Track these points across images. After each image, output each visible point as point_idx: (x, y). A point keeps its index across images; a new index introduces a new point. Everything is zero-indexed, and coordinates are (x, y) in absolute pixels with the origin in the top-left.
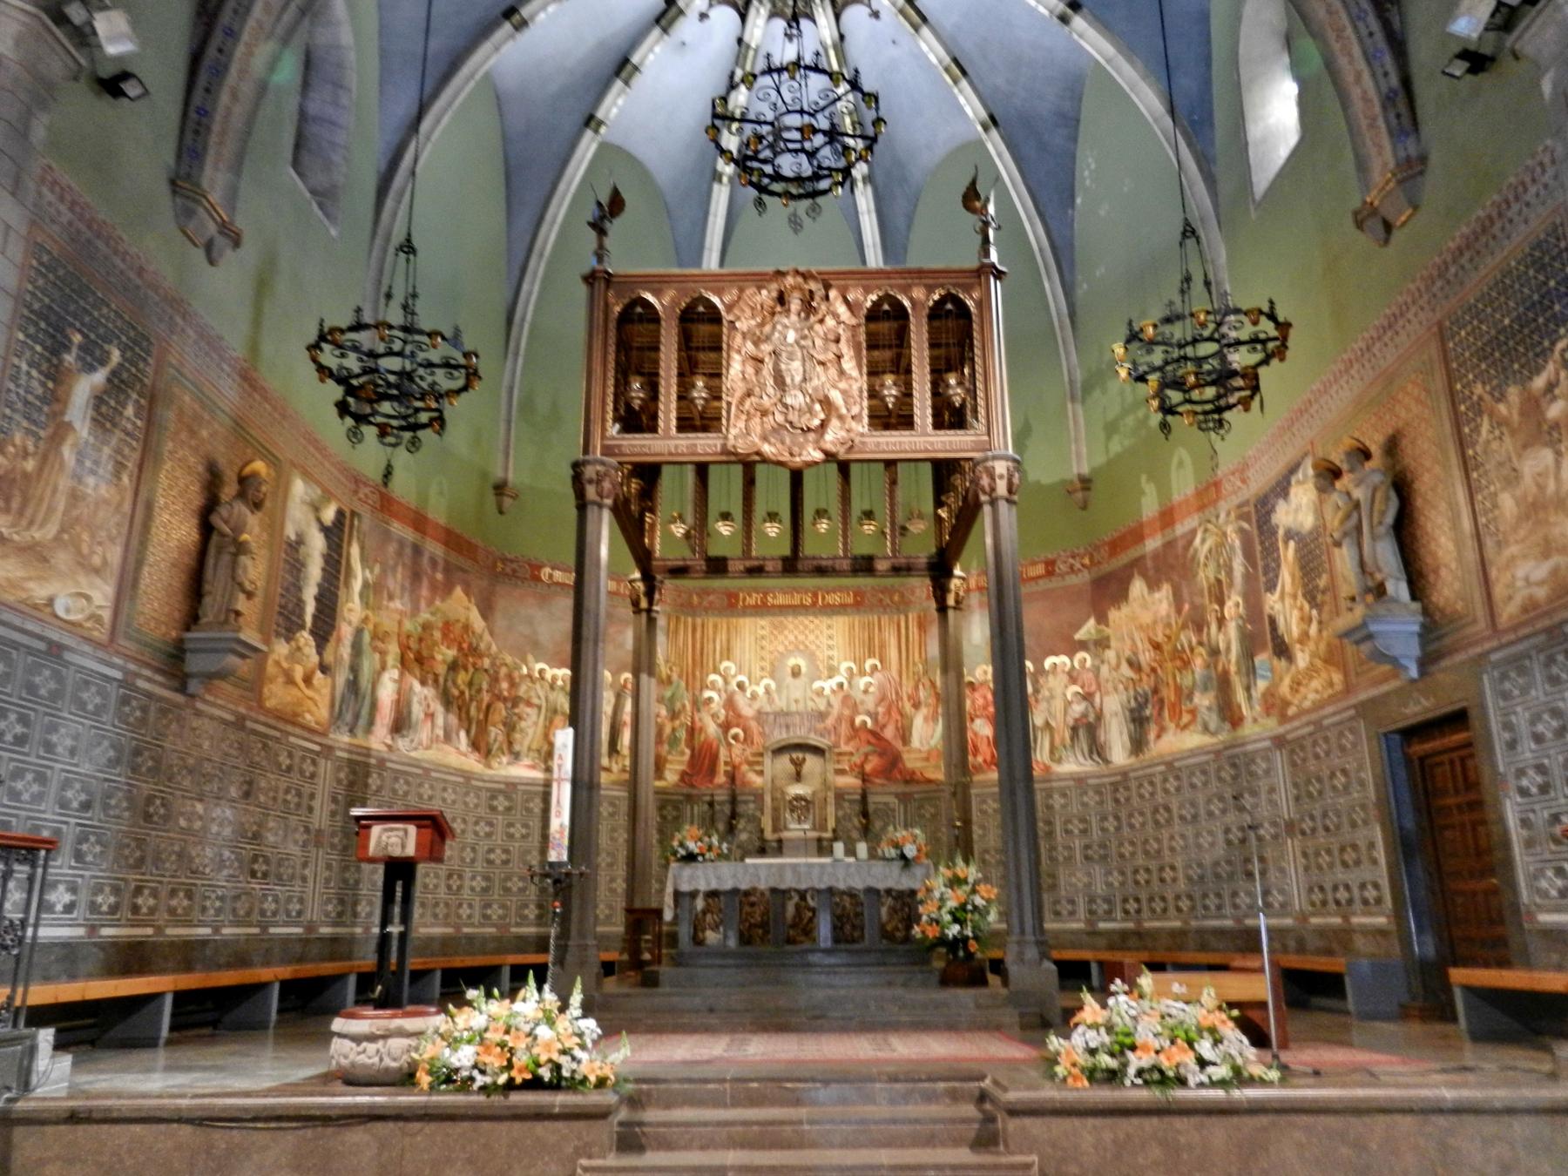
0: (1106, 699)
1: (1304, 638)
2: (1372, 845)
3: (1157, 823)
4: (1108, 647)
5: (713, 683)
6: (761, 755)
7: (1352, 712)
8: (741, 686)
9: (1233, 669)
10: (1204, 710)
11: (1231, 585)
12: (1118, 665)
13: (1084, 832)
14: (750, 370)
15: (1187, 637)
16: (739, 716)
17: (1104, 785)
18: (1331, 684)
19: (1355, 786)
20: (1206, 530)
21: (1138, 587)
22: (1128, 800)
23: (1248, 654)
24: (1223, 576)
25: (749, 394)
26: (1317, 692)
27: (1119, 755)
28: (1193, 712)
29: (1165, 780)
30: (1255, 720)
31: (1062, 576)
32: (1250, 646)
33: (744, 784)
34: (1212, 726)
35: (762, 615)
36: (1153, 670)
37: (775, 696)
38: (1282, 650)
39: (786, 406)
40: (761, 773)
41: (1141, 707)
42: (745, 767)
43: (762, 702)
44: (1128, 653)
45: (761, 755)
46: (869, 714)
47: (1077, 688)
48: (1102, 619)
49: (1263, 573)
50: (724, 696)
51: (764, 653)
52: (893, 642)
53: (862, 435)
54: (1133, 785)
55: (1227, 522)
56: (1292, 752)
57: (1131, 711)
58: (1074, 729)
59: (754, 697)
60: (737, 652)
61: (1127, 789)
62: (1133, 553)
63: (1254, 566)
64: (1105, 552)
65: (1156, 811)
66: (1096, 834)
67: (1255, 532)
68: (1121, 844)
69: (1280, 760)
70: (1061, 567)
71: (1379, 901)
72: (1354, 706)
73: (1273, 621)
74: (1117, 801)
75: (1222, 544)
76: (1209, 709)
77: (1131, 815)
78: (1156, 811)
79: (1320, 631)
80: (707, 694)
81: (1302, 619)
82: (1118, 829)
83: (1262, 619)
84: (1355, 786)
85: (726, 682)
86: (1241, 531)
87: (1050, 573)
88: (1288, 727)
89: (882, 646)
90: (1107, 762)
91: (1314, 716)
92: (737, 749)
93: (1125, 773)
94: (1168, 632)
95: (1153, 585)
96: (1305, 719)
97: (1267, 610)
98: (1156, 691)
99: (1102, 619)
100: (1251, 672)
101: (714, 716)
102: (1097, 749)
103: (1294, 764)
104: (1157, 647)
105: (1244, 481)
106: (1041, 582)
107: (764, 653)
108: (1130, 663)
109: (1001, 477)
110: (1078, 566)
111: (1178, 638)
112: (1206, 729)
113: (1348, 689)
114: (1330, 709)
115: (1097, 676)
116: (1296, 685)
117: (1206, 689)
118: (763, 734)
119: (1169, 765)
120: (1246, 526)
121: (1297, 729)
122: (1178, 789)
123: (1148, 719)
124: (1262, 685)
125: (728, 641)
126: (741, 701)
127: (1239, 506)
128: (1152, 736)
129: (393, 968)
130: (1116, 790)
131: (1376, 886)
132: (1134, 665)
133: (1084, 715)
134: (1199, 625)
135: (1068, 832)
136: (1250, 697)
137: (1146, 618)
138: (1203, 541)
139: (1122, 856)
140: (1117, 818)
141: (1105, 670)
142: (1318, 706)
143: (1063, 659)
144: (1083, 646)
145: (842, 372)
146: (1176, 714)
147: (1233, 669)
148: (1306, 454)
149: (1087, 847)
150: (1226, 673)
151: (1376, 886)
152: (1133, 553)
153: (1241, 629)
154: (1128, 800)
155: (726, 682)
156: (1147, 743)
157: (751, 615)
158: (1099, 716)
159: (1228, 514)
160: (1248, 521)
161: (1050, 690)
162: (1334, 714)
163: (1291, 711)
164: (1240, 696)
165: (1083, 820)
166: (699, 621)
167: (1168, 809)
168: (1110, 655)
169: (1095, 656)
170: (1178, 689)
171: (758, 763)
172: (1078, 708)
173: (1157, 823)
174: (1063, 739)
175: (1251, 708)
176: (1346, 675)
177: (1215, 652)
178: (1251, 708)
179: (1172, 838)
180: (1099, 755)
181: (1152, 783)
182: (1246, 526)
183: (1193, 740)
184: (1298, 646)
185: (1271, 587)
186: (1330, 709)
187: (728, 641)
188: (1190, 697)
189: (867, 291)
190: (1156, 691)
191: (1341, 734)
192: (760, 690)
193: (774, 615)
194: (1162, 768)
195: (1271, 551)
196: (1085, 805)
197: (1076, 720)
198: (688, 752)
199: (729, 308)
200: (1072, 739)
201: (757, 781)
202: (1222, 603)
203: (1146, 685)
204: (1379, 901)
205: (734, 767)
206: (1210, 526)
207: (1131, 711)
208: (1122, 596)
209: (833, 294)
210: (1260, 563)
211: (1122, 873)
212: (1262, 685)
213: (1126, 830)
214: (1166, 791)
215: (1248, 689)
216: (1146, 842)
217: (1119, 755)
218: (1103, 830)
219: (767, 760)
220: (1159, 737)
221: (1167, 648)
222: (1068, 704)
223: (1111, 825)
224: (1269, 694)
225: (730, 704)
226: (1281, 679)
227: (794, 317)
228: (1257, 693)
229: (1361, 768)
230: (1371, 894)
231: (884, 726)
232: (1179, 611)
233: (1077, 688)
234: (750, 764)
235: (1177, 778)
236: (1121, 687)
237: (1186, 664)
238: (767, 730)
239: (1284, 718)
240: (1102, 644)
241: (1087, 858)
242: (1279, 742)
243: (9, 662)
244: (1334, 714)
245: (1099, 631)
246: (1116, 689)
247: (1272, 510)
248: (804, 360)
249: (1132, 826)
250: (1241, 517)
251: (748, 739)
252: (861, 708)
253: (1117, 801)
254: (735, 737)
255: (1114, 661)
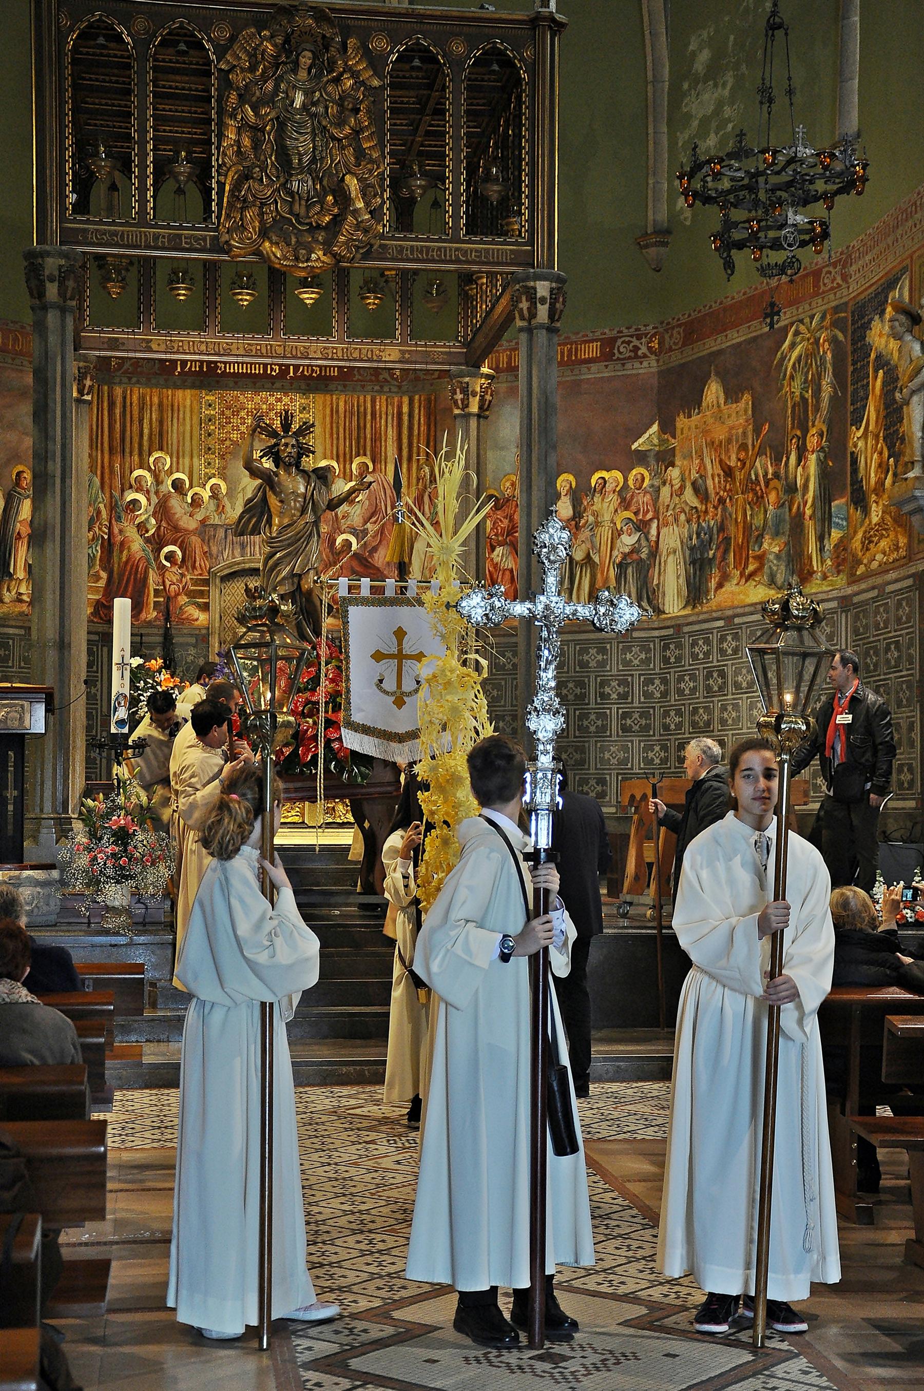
0: (664, 531)
1: (880, 488)
2: (911, 728)
3: (708, 688)
4: (673, 464)
5: (139, 479)
6: (206, 582)
7: (910, 582)
8: (177, 485)
9: (808, 512)
10: (771, 557)
11: (817, 409)
12: (682, 488)
13: (623, 696)
14: (246, 142)
15: (763, 466)
16: (176, 528)
17: (651, 639)
18: (897, 548)
19: (905, 664)
20: (797, 333)
21: (713, 391)
22: (679, 659)
23: (826, 497)
24: (809, 395)
25: (246, 176)
26: (884, 553)
27: (673, 604)
28: (761, 558)
29: (723, 639)
30: (825, 577)
31: (623, 361)
32: (829, 486)
33: (182, 621)
34: (780, 579)
35: (210, 388)
36: (722, 501)
37: (226, 501)
38: (860, 500)
39: (291, 193)
40: (205, 607)
41: (704, 546)
42: (183, 599)
43: (208, 508)
44: (694, 475)
45: (206, 582)
46: (354, 532)
47: (628, 514)
48: (668, 427)
49: (847, 412)
50: (155, 500)
51: (211, 442)
52: (391, 433)
53: (382, 236)
54: (687, 641)
55: (820, 328)
56: (856, 618)
57: (692, 549)
58: (622, 567)
59: (196, 502)
60: (173, 437)
61: (679, 646)
62: (713, 344)
63: (844, 392)
64: (677, 335)
65: (709, 675)
66: (637, 699)
67: (849, 348)
68: (666, 714)
69: (844, 622)
70: (624, 350)
71: (912, 783)
72: (912, 576)
73: (854, 462)
74: (666, 660)
75: (811, 354)
76: (778, 557)
77: (681, 679)
78: (709, 675)
79: (894, 482)
80: (130, 496)
81: (880, 465)
82: (665, 694)
83: (845, 454)
84: (905, 664)
85: (158, 482)
86: (834, 341)
87: (607, 356)
88: (855, 588)
89: (377, 438)
90: (659, 611)
91: (879, 580)
92: (173, 573)
93: (678, 626)
94: (742, 455)
95: (732, 395)
96: (871, 582)
97: (851, 448)
98: (722, 528)
99: (668, 427)
100: (825, 520)
101: (142, 528)
102: (647, 595)
103: (856, 632)
104: (729, 472)
105: (845, 278)
106: (594, 367)
107: (211, 442)
108: (696, 489)
109: (543, 300)
110: (643, 350)
111: (753, 466)
112: (772, 582)
113: (910, 558)
114: (892, 575)
115: (656, 500)
116: (868, 541)
117: (777, 534)
118: (207, 554)
119: (729, 619)
120: (841, 336)
121: (863, 592)
122: (736, 651)
123: (711, 561)
124: (836, 534)
125: (161, 422)
126: (177, 506)
127: (836, 310)
128: (713, 584)
129: (10, 833)
130: (666, 647)
131: (911, 770)
132: (700, 491)
133: (635, 550)
134: (778, 456)
135: (603, 696)
136: (822, 549)
137: (720, 434)
138: (793, 346)
139: (666, 727)
140: (665, 681)
141: (665, 491)
142: (884, 569)
143: (614, 477)
144: (641, 458)
145: (360, 154)
146: (742, 562)
147: (808, 512)
148: (904, 270)
149: (625, 715)
150: (800, 515)
151: (911, 770)
152: (713, 344)
153: (821, 464)
154: (679, 659)
155: (158, 482)
156: (707, 592)
157: (193, 386)
158: (654, 553)
159: (823, 318)
160: (844, 332)
161: (596, 515)
162: (897, 581)
163: (861, 570)
164: (812, 547)
165: (623, 683)
166: (118, 391)
167: (722, 674)
168: (674, 473)
169: (656, 474)
170: (748, 528)
171: (201, 594)
172: (628, 540)
173: (708, 688)
174: (607, 579)
175: (823, 562)
176: (910, 537)
177: (791, 489)
178: (823, 562)
179: (724, 708)
180: (650, 602)
181: (707, 641)
182: (841, 336)
183: (758, 593)
184: (874, 498)
185: (857, 421)
186: (892, 575)
187: (161, 422)
188: (759, 539)
189: (394, 42)
190: (722, 528)
191: (899, 605)
192: (206, 494)
193: (226, 388)
194: (721, 623)
195: (861, 376)
196: (627, 663)
197: (625, 556)
198: (104, 575)
199: (221, 52)
200: (618, 579)
201: (202, 618)
202: (805, 431)
203: (711, 521)
204: (912, 783)
205: (169, 599)
206: (802, 328)
207: (692, 549)
208: (693, 401)
209: (352, 42)
210: (850, 389)
211: (664, 748)
212: (836, 534)
213: (673, 697)
214: (722, 652)
215: (821, 538)
216: (695, 710)
217: (673, 604)
218: (648, 695)
219: (214, 593)
220: (720, 586)
221: (739, 476)
222: (617, 534)
223: (656, 688)
224: (842, 545)
225: (162, 510)
226: (855, 532)
227: (303, 74)
228: (829, 545)
229: (911, 644)
230: (906, 777)
231: (375, 549)
232: (757, 431)
233: (628, 514)
234: (191, 594)
235: (736, 637)
236: (683, 517)
237: (760, 499)
238: (214, 550)
239: (853, 579)
240: (666, 458)
241: (625, 729)
242: (845, 603)
243: (6, 646)
244: (897, 581)
245: (662, 442)
246: (676, 520)
247: (867, 326)
248: (314, 134)
249: (680, 692)
250: (835, 324)
251: (187, 561)
252: (344, 524)
253: (666, 660)
254: (170, 557)
255: (677, 484)
